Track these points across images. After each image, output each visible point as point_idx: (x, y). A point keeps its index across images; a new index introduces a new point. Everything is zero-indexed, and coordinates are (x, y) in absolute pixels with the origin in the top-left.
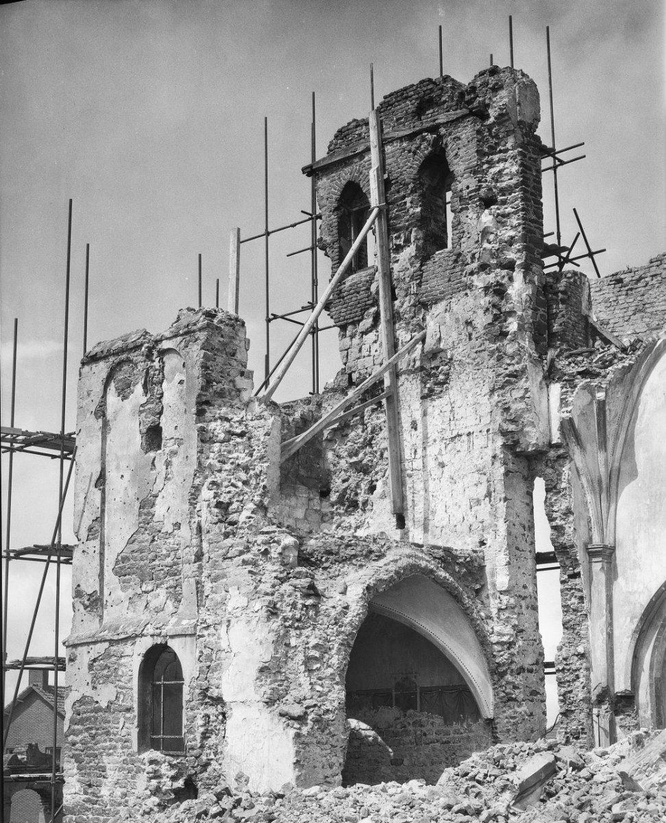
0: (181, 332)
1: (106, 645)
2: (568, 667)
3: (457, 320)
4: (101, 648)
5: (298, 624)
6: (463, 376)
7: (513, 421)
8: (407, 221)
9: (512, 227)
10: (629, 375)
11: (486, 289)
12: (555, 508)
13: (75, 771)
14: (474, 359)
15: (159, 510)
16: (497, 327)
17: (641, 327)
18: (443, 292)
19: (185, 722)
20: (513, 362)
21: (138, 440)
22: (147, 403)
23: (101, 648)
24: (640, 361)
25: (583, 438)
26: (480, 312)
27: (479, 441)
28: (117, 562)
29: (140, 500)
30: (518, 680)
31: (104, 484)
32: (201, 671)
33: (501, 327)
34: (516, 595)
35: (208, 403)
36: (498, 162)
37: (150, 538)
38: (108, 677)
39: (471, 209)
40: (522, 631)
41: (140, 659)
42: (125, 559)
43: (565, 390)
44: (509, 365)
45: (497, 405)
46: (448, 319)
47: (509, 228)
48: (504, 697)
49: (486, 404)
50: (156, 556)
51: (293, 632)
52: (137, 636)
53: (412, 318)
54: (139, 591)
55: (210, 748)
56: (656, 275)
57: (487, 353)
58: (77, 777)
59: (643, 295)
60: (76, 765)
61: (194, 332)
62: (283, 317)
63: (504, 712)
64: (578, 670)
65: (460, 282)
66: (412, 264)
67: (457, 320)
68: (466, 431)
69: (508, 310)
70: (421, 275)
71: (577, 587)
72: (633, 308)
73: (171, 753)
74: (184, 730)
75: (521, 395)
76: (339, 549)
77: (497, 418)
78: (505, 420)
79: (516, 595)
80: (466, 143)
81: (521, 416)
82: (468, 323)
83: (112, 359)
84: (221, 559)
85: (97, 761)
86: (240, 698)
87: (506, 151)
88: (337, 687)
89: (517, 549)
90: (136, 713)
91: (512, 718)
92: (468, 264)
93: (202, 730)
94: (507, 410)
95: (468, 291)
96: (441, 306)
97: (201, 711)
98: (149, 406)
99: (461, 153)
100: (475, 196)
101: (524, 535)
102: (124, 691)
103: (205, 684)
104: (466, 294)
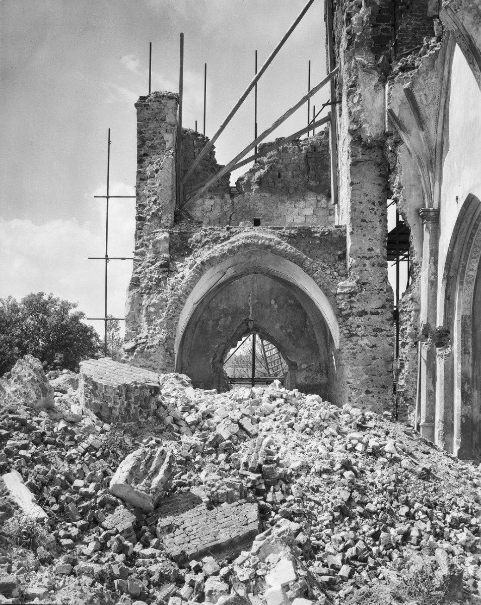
2: (405, 310)
5: (149, 290)
10: (439, 60)
25: (405, 123)
30: (359, 320)
34: (359, 257)
35: (146, 155)
40: (365, 284)
48: (347, 333)
51: (145, 296)
62: (254, 83)
63: (347, 344)
76: (201, 239)
79: (359, 257)
81: (359, 117)
88: (163, 331)
89: (364, 221)
91: (352, 349)
101: (373, 209)
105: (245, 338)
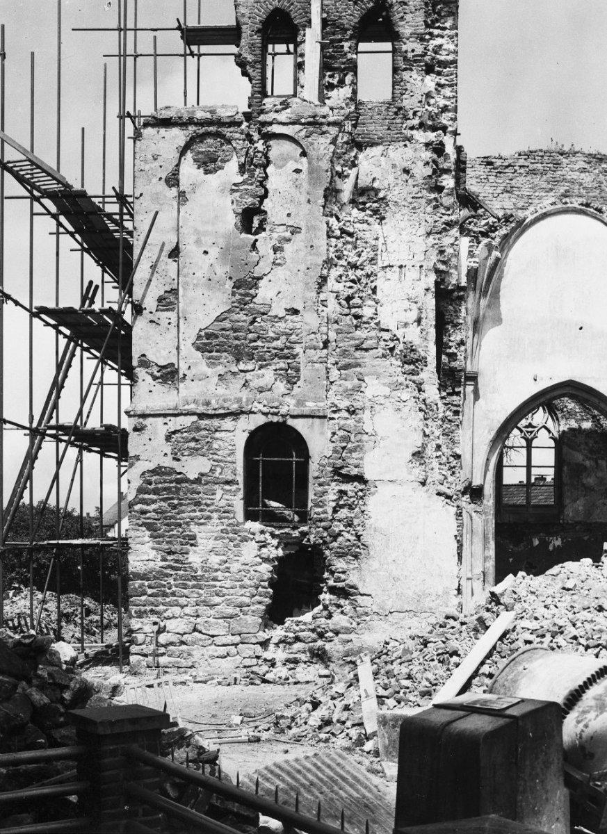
0: (303, 121)
1: (195, 418)
3: (394, 166)
4: (188, 421)
6: (398, 216)
7: (444, 263)
8: (343, 63)
9: (444, 97)
11: (427, 145)
12: (452, 339)
13: (147, 539)
14: (411, 203)
15: (265, 292)
16: (434, 180)
17: (508, 204)
18: (381, 138)
19: (311, 496)
20: (448, 213)
21: (231, 221)
22: (244, 183)
23: (188, 421)
24: (513, 230)
26: (421, 164)
27: (412, 274)
28: (199, 337)
29: (234, 280)
31: (177, 256)
32: (335, 451)
33: (436, 181)
36: (437, 36)
37: (250, 318)
38: (197, 450)
39: (415, 71)
41: (246, 435)
42: (208, 336)
43: (472, 244)
44: (444, 214)
45: (433, 246)
46: (383, 163)
47: (442, 97)
49: (421, 244)
50: (259, 337)
52: (243, 412)
53: (345, 153)
54: (235, 369)
55: (339, 521)
56: (523, 166)
57: (423, 201)
58: (151, 544)
59: (511, 180)
60: (148, 533)
61: (322, 124)
64: (454, 467)
65: (401, 133)
66: (347, 105)
67: (394, 166)
68: (399, 264)
69: (445, 167)
70: (358, 118)
71: (454, 403)
72: (502, 188)
73: (275, 524)
74: (310, 504)
75: (452, 242)
77: (432, 257)
78: (439, 261)
80: (414, 10)
82: (406, 171)
83: (192, 128)
84: (354, 349)
85: (181, 530)
86: (388, 477)
87: (444, 29)
90: (241, 486)
92: (409, 119)
93: (334, 504)
94: (442, 252)
95: (407, 143)
96: (377, 150)
97: (334, 487)
98: (246, 187)
99: (408, 17)
100: (420, 61)
102: (222, 464)
103: (339, 463)
104: (405, 146)
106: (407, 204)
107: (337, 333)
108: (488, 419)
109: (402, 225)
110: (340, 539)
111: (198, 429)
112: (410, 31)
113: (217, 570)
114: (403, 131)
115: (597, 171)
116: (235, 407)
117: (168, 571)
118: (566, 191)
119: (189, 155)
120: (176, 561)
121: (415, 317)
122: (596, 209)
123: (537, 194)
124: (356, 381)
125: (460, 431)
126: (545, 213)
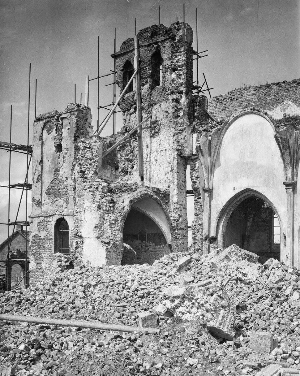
1: (43, 218)
3: (163, 110)
6: (164, 130)
7: (181, 146)
8: (147, 75)
10: (220, 131)
12: (194, 176)
13: (33, 259)
14: (168, 124)
15: (61, 172)
21: (54, 149)
23: (42, 219)
24: (223, 127)
26: (171, 108)
27: (169, 152)
28: (47, 190)
32: (75, 227)
35: (78, 136)
38: (44, 228)
40: (181, 216)
44: (180, 127)
49: (172, 140)
53: (148, 109)
55: (78, 252)
61: (73, 111)
64: (199, 229)
66: (148, 91)
70: (151, 95)
74: (69, 246)
78: (178, 146)
87: (181, 52)
88: (120, 233)
89: (181, 189)
90: (53, 240)
93: (75, 246)
94: (179, 142)
95: (167, 101)
97: (75, 240)
98: (58, 137)
104: (166, 102)
105: (15, 231)
106: (167, 125)
107: (78, 185)
108: (217, 208)
109: (166, 133)
110: (78, 259)
111: (44, 221)
112: (166, 57)
113: (48, 270)
114: (165, 96)
115: (259, 93)
116: (51, 213)
117: (37, 270)
118: (246, 105)
119: (45, 129)
120: (39, 266)
121: (170, 170)
122: (257, 111)
123: (235, 109)
124: (83, 201)
125: (203, 214)
126: (237, 117)
